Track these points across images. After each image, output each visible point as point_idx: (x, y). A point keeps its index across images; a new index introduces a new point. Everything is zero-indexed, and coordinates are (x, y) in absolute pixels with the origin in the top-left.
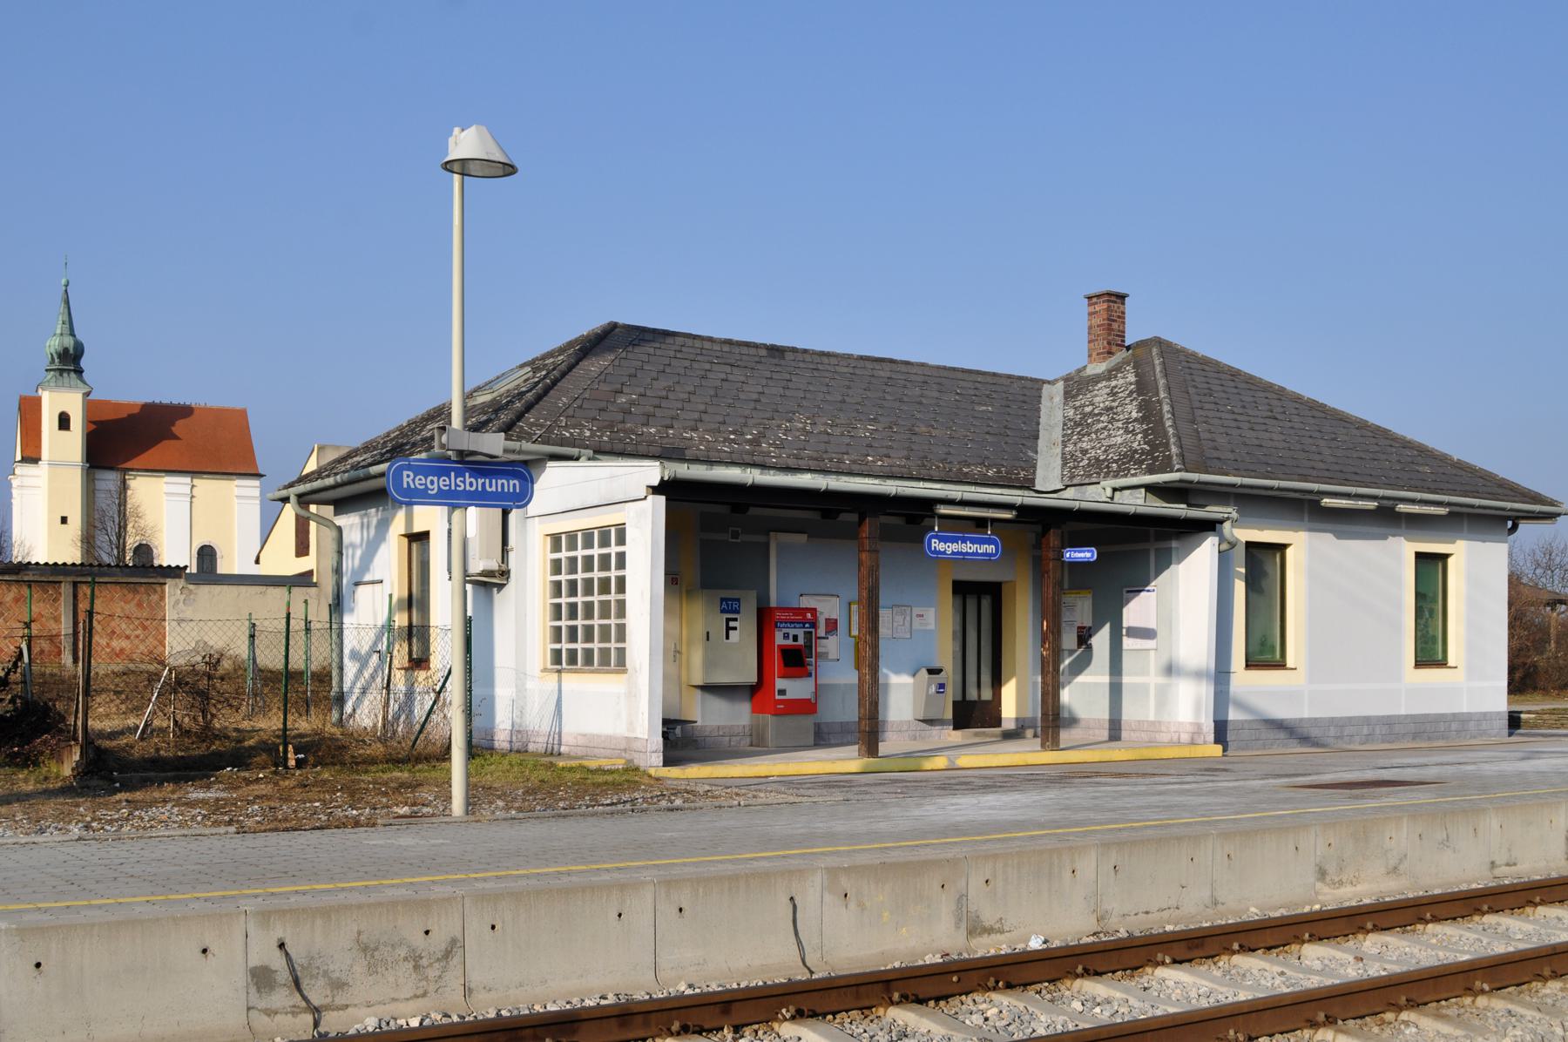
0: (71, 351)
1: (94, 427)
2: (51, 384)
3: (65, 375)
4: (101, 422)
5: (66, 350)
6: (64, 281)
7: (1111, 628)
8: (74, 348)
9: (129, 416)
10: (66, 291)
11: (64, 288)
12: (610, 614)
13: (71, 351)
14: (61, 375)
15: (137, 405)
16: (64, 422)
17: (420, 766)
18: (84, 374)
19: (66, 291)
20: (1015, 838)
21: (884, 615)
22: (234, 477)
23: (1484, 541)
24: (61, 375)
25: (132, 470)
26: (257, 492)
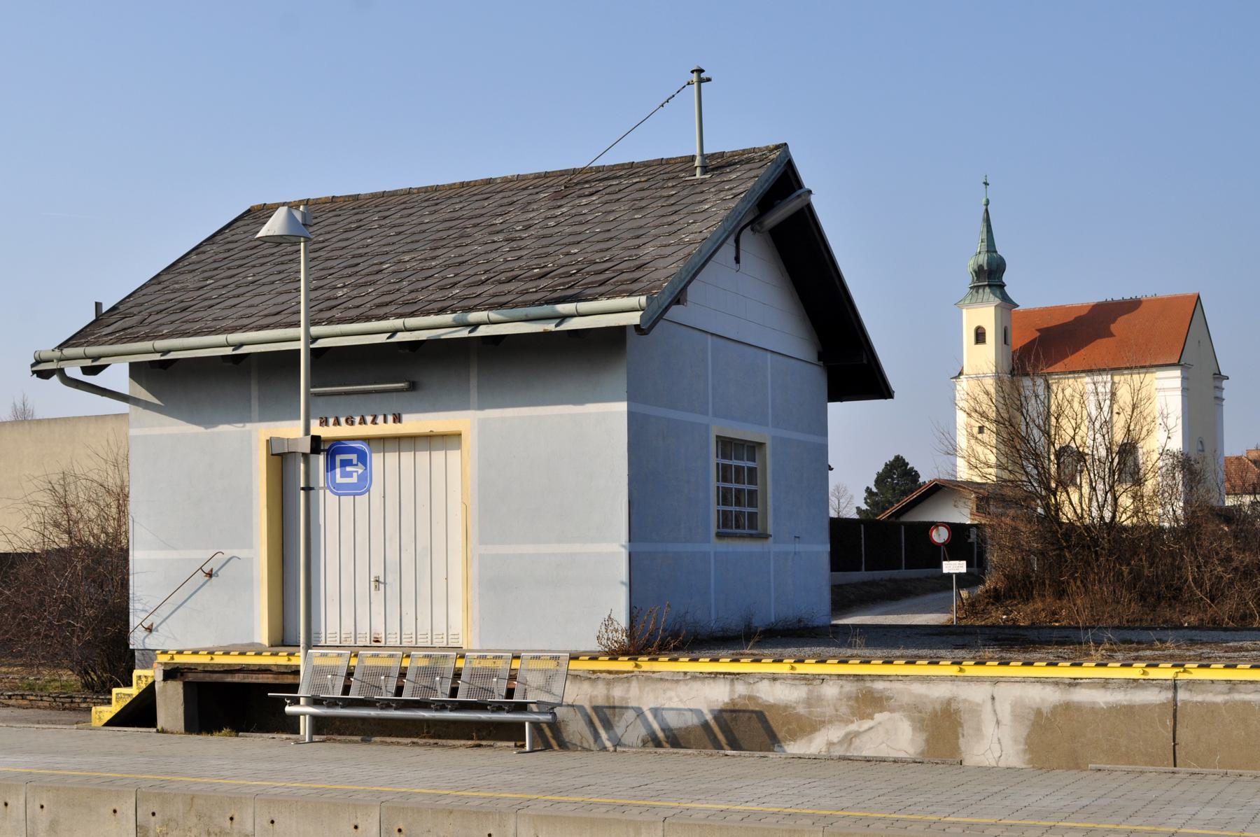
0: (986, 268)
1: (1038, 334)
2: (966, 302)
3: (981, 291)
4: (1047, 329)
5: (980, 267)
6: (984, 201)
7: (298, 221)
8: (988, 263)
9: (1076, 319)
10: (987, 210)
11: (984, 207)
12: (902, 565)
13: (986, 268)
14: (977, 292)
15: (1188, 297)
16: (980, 336)
17: (879, 696)
18: (1005, 288)
19: (987, 210)
20: (69, 770)
21: (675, 712)
22: (1154, 369)
23: (102, 396)
24: (977, 292)
25: (1057, 374)
26: (1178, 383)
